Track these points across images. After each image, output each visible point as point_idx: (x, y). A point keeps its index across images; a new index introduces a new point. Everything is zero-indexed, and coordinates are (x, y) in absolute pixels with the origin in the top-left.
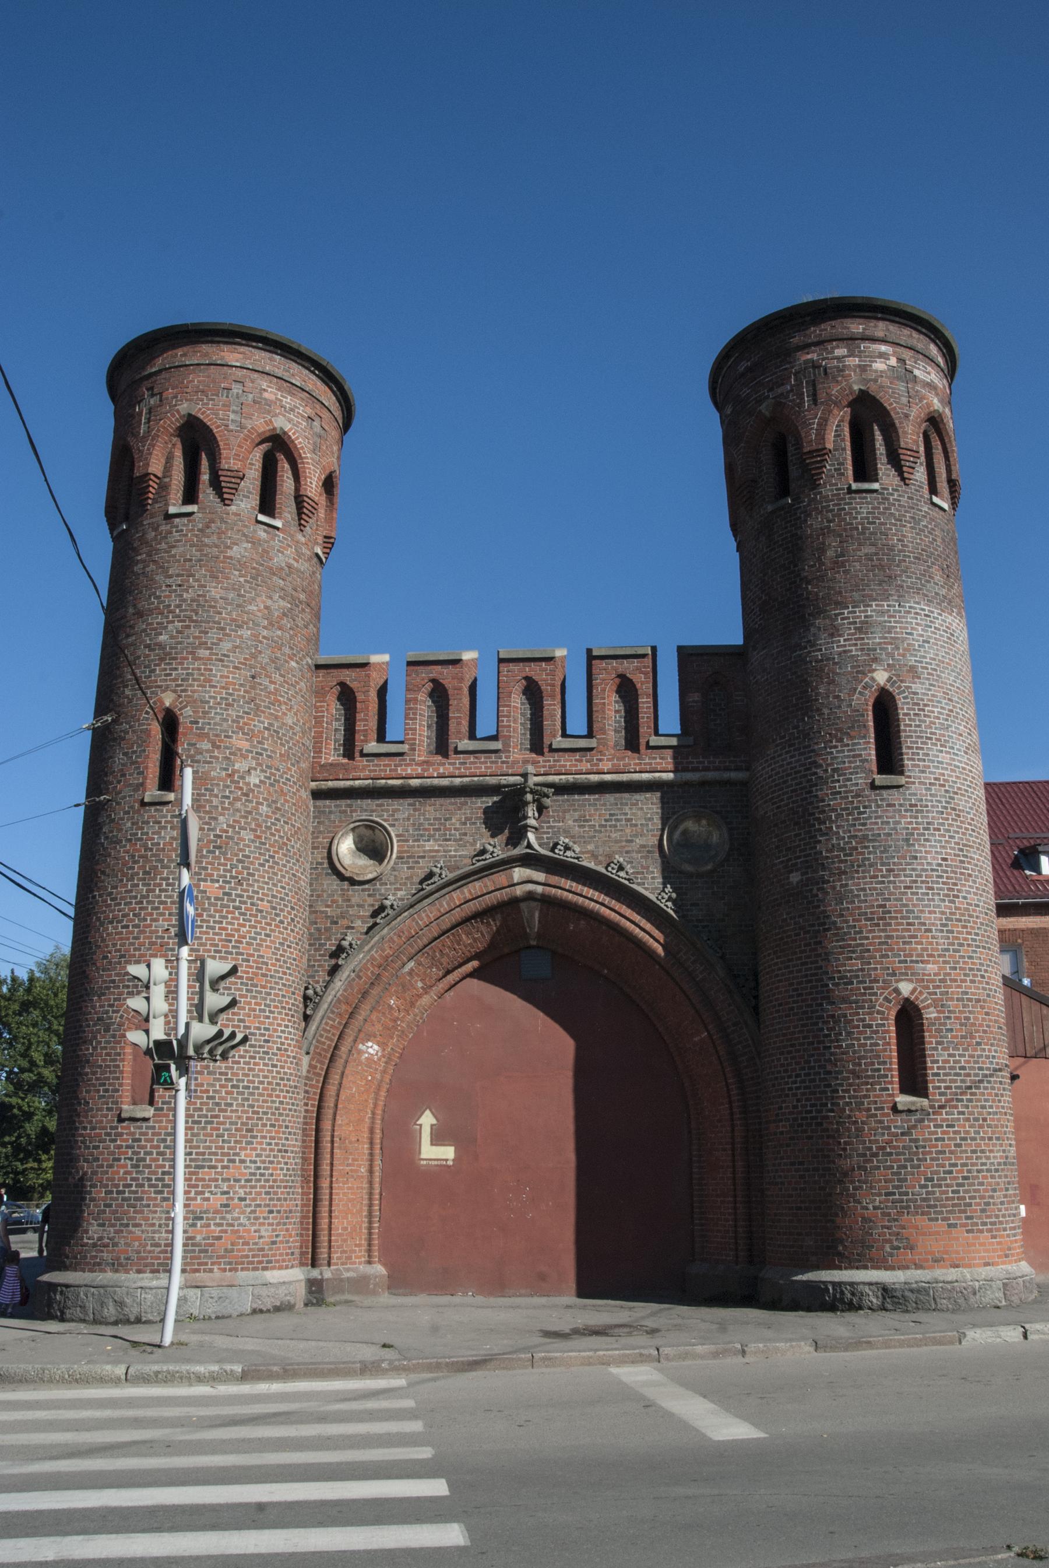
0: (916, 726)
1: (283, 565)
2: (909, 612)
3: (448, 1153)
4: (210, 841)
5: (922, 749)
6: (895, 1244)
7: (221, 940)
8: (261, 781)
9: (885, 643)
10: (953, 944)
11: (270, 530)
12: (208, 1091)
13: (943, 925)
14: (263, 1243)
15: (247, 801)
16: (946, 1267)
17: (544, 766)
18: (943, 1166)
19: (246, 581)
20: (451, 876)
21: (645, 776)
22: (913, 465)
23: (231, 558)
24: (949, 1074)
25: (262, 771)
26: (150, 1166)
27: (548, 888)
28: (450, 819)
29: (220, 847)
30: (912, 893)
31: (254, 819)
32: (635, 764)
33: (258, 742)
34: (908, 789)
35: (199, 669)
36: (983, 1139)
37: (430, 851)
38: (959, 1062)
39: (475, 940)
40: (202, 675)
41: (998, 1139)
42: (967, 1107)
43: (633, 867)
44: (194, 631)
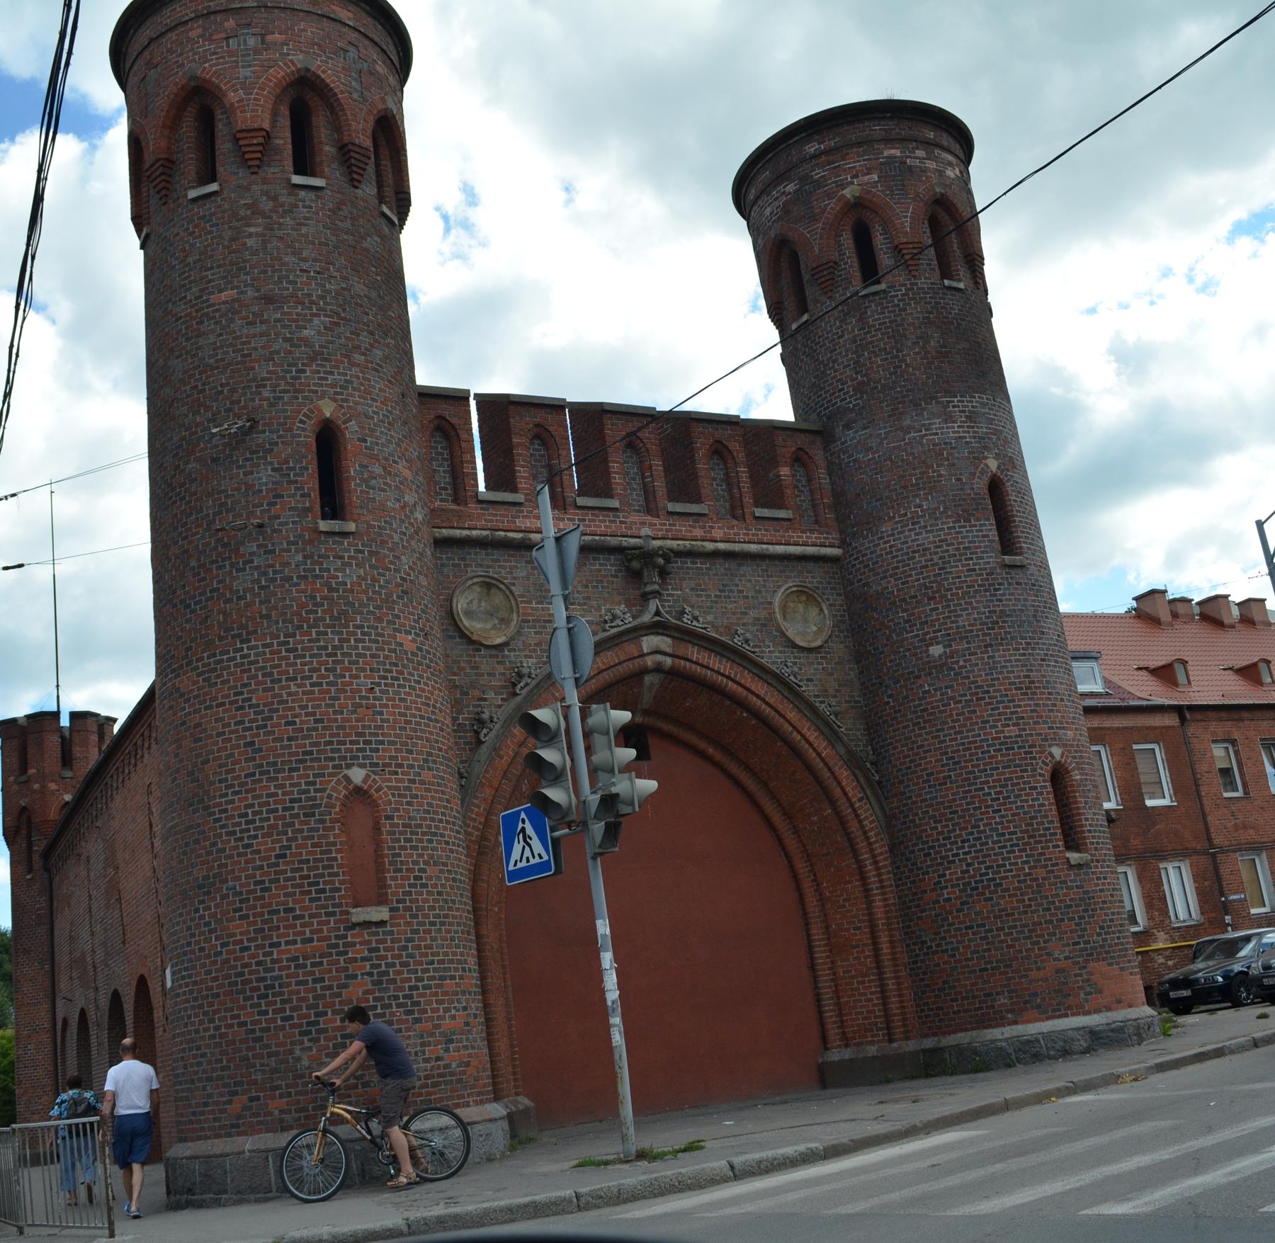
6: (1088, 989)
21: (753, 548)
27: (677, 661)
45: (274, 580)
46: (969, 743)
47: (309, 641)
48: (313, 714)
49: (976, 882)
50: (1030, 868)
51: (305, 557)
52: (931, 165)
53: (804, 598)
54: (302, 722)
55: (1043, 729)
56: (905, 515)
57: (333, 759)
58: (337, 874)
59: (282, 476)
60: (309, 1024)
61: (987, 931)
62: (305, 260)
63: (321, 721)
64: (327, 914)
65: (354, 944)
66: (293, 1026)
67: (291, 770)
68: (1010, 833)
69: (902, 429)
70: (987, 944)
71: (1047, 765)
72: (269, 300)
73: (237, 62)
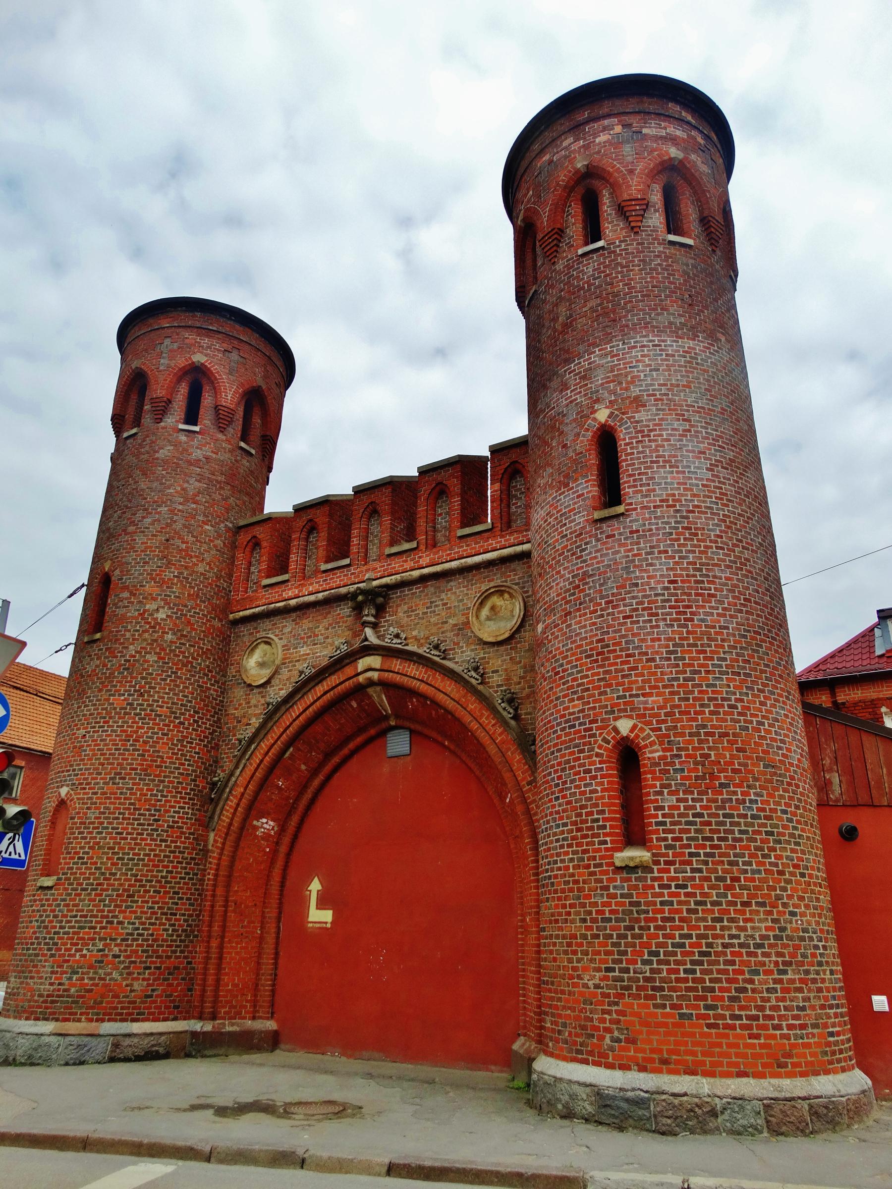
1: (201, 457)
2: (635, 347)
3: (327, 916)
6: (616, 1034)
8: (167, 616)
11: (191, 434)
12: (96, 863)
14: (135, 997)
15: (153, 632)
16: (676, 1072)
18: (672, 937)
21: (454, 564)
23: (157, 459)
25: (170, 608)
31: (158, 645)
33: (168, 587)
34: (629, 516)
36: (730, 903)
37: (304, 655)
42: (706, 863)
44: (128, 515)
53: (506, 596)
71: (608, 742)
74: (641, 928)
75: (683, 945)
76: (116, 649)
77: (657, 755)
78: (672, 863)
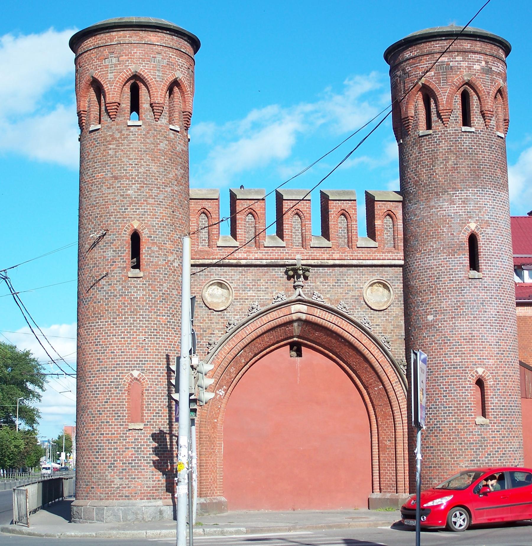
0: (488, 250)
4: (160, 296)
5: (490, 260)
7: (167, 344)
8: (179, 265)
9: (475, 209)
10: (501, 351)
13: (496, 342)
17: (307, 255)
18: (495, 449)
19: (167, 162)
20: (263, 309)
22: (490, 118)
24: (498, 409)
26: (143, 451)
28: (260, 280)
29: (164, 299)
30: (484, 328)
32: (350, 256)
34: (483, 279)
35: (150, 209)
36: (511, 437)
38: (502, 403)
39: (270, 339)
40: (151, 212)
41: (517, 437)
43: (348, 306)
45: (110, 296)
46: (438, 363)
47: (122, 321)
48: (121, 349)
49: (432, 427)
50: (456, 424)
51: (122, 287)
52: (464, 64)
54: (117, 352)
55: (474, 359)
56: (426, 250)
57: (127, 367)
58: (125, 411)
59: (116, 253)
60: (111, 464)
61: (433, 450)
62: (132, 159)
63: (123, 352)
64: (120, 425)
65: (129, 437)
66: (106, 464)
67: (112, 370)
68: (449, 407)
69: (430, 207)
70: (433, 456)
72: (116, 178)
73: (107, 71)
74: (485, 446)
75: (498, 451)
76: (156, 285)
77: (491, 383)
78: (496, 423)
